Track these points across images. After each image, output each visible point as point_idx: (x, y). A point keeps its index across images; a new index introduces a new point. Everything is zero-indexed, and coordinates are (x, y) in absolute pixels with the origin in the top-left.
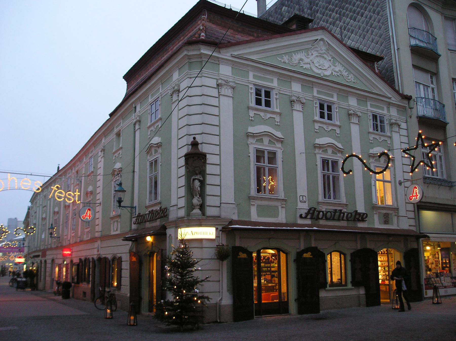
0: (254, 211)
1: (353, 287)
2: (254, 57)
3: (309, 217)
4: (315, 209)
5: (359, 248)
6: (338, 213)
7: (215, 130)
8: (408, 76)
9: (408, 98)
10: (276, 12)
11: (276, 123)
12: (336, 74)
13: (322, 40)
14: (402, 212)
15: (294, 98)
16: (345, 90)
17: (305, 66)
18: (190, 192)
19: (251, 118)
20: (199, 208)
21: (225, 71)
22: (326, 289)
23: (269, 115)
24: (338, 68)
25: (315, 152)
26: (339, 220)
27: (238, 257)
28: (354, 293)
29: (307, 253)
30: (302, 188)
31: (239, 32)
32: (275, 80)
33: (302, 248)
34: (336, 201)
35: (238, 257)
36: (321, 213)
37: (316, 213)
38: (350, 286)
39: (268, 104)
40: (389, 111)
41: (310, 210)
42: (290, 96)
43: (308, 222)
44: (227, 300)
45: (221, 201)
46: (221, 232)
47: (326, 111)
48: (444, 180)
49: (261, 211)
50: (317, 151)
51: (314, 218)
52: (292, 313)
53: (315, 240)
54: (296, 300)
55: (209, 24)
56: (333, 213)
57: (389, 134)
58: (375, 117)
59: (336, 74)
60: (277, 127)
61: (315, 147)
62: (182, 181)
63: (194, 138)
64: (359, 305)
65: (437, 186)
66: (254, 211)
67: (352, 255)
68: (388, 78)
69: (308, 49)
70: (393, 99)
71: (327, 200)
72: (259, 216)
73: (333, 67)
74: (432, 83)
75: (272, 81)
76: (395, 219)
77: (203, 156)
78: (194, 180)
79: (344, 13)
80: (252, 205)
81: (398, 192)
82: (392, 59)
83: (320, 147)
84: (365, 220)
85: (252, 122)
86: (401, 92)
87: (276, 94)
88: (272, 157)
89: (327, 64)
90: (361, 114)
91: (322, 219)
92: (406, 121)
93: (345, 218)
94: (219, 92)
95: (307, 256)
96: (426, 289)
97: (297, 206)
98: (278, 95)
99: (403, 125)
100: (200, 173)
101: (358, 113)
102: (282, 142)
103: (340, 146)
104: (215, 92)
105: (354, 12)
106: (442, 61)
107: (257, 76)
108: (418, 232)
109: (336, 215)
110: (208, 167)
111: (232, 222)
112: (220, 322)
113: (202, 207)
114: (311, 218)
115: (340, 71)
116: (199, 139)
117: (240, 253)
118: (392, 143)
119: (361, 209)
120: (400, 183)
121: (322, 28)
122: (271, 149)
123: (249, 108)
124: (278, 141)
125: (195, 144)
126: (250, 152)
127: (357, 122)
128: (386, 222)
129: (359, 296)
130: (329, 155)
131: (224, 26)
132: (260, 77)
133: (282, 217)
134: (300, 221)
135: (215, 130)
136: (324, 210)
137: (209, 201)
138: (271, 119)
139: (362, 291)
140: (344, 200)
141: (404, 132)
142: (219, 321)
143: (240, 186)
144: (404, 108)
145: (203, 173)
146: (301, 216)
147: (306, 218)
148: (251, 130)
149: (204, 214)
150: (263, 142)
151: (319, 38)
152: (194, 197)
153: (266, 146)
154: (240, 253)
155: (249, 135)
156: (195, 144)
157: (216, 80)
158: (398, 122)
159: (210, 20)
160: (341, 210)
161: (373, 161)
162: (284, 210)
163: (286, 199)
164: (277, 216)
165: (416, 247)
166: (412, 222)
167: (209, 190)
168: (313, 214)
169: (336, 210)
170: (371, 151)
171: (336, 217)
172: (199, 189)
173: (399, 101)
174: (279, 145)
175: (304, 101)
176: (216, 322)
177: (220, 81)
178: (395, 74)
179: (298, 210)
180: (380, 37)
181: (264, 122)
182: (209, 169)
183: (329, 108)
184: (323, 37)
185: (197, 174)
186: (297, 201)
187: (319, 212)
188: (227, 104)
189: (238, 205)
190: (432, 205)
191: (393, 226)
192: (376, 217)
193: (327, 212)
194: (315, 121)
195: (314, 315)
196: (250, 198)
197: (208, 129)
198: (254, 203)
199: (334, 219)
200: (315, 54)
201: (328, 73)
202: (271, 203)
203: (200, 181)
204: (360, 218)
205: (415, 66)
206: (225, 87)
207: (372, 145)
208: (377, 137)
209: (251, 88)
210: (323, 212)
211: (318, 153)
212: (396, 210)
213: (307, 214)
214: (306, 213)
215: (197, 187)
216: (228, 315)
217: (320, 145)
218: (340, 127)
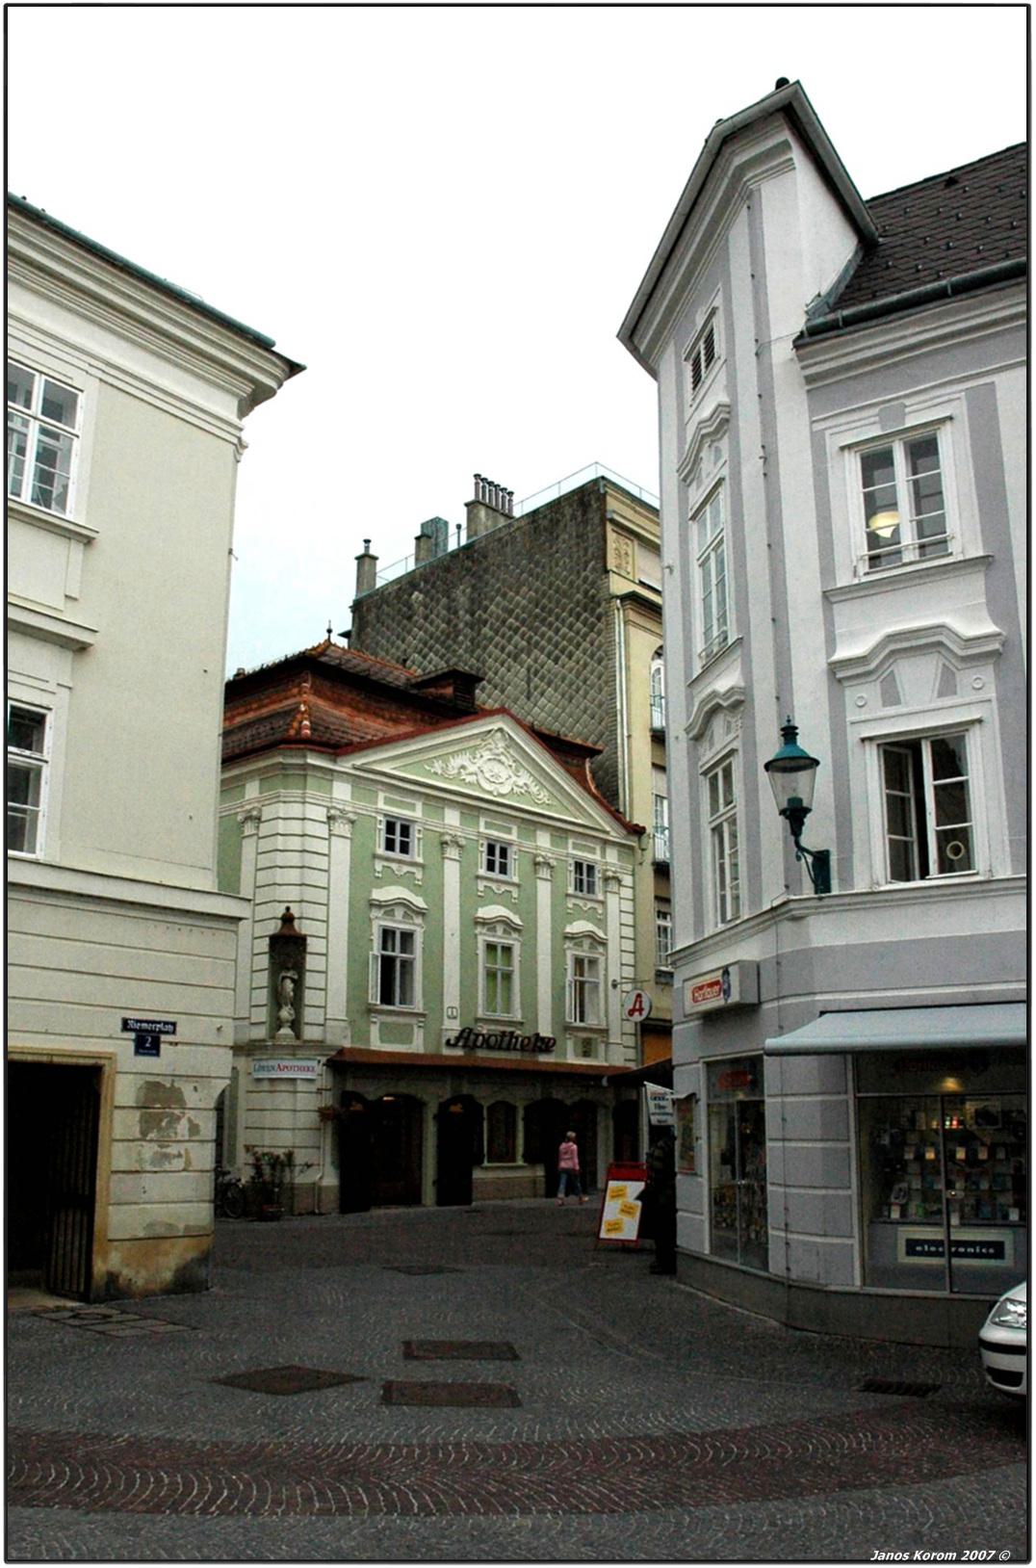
0: (374, 1031)
2: (386, 768)
5: (539, 1097)
7: (321, 895)
9: (638, 831)
10: (398, 597)
13: (500, 730)
14: (615, 1037)
15: (447, 838)
16: (531, 822)
17: (469, 779)
18: (277, 999)
21: (342, 791)
24: (524, 779)
26: (508, 1049)
28: (527, 1173)
30: (452, 997)
31: (359, 710)
32: (419, 805)
33: (448, 1096)
34: (505, 1017)
38: (520, 1162)
39: (405, 848)
40: (603, 855)
42: (442, 834)
43: (459, 1052)
44: (330, 1179)
47: (497, 856)
49: (386, 1033)
50: (479, 929)
55: (312, 699)
57: (600, 897)
58: (579, 866)
60: (416, 889)
61: (477, 923)
62: (263, 979)
66: (374, 1031)
67: (526, 1109)
68: (607, 793)
69: (476, 747)
71: (490, 1015)
75: (412, 807)
76: (602, 1047)
77: (300, 941)
79: (537, 643)
85: (380, 882)
88: (407, 937)
89: (504, 773)
99: (628, 880)
103: (518, 921)
104: (322, 830)
105: (556, 646)
109: (504, 1041)
110: (308, 958)
111: (341, 1051)
113: (296, 1025)
116: (295, 911)
118: (605, 913)
119: (545, 1031)
120: (615, 986)
121: (502, 711)
123: (375, 856)
124: (516, 930)
125: (288, 919)
128: (586, 1054)
129: (534, 1182)
131: (338, 702)
133: (417, 1044)
134: (446, 1051)
135: (321, 895)
137: (309, 1014)
139: (540, 1172)
140: (518, 1016)
143: (356, 988)
144: (631, 848)
145: (299, 967)
146: (448, 1043)
147: (455, 1045)
149: (298, 1036)
151: (495, 727)
153: (399, 924)
155: (373, 905)
156: (288, 919)
159: (317, 692)
164: (409, 1040)
167: (309, 997)
169: (504, 1033)
170: (569, 929)
174: (418, 920)
180: (600, 706)
181: (397, 880)
182: (311, 962)
183: (504, 853)
184: (500, 725)
188: (342, 850)
192: (570, 1045)
196: (370, 1010)
197: (310, 894)
199: (500, 1048)
200: (487, 755)
201: (505, 790)
202: (402, 1020)
203: (293, 981)
207: (570, 918)
208: (581, 903)
212: (605, 1032)
213: (458, 1039)
216: (331, 1201)
218: (518, 886)
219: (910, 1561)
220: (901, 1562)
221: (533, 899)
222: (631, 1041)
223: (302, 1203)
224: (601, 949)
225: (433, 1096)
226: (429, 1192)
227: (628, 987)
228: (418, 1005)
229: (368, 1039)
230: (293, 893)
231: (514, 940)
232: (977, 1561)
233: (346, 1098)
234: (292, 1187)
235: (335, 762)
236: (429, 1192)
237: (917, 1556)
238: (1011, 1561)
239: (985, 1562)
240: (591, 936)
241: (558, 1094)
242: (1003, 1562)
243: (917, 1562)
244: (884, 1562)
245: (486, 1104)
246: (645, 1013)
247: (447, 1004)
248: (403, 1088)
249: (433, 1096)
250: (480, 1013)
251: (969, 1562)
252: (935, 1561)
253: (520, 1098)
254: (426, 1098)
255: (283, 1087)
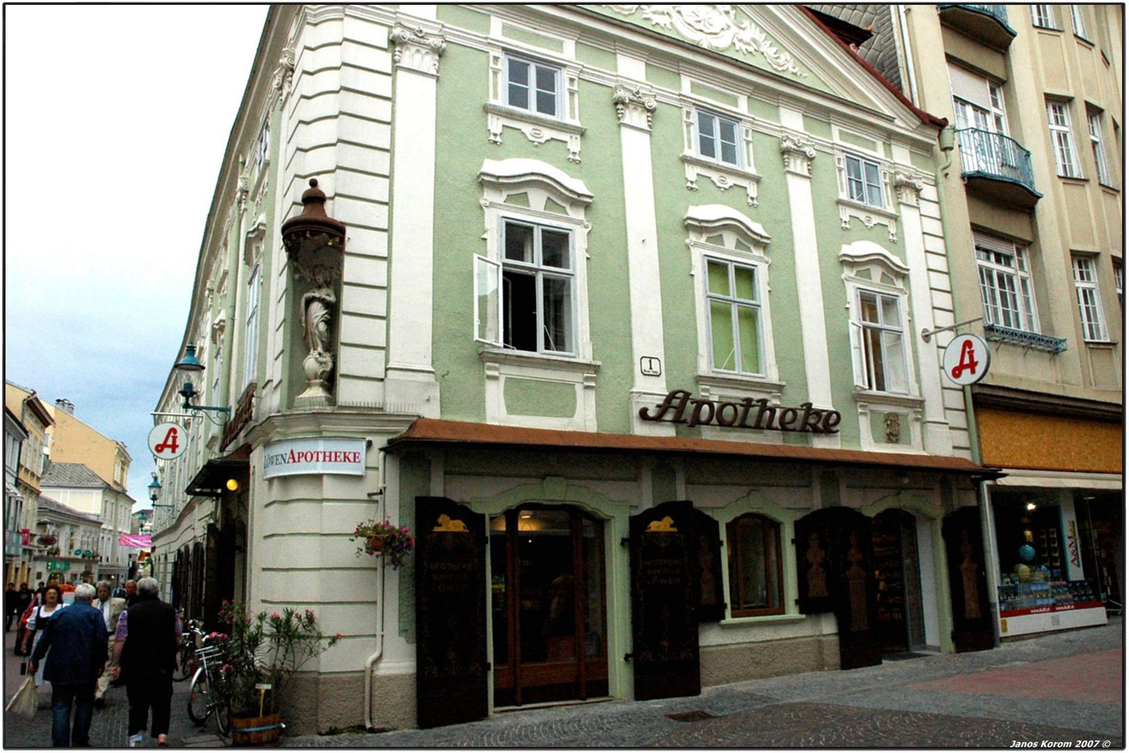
1: (804, 616)
3: (669, 416)
4: (687, 395)
6: (757, 409)
8: (936, 80)
9: (939, 125)
11: (571, 156)
12: (744, 47)
14: (934, 411)
16: (771, 88)
18: (300, 338)
19: (492, 138)
20: (322, 385)
22: (723, 622)
23: (547, 134)
25: (687, 241)
26: (758, 427)
27: (437, 529)
28: (806, 630)
29: (660, 519)
30: (648, 336)
33: (647, 503)
34: (748, 376)
35: (437, 529)
36: (706, 408)
37: (690, 407)
38: (792, 612)
41: (672, 396)
43: (665, 431)
44: (398, 661)
45: (387, 362)
46: (382, 454)
48: (1033, 337)
49: (517, 397)
50: (693, 237)
51: (685, 421)
52: (618, 695)
53: (689, 482)
54: (627, 657)
56: (740, 409)
57: (891, 210)
59: (744, 47)
60: (574, 164)
61: (688, 228)
63: (314, 184)
64: (821, 666)
65: (1020, 350)
67: (797, 525)
68: (887, 75)
70: (897, 121)
72: (511, 410)
73: (734, 29)
74: (995, 104)
76: (915, 429)
78: (309, 302)
80: (489, 377)
81: (922, 360)
82: (892, 36)
83: (700, 227)
84: (834, 429)
86: (917, 105)
87: (572, 80)
90: (814, 153)
91: (707, 423)
92: (936, 181)
93: (776, 423)
94: (394, 62)
95: (662, 529)
96: (1004, 614)
97: (632, 387)
98: (576, 83)
99: (929, 192)
100: (328, 284)
101: (806, 149)
102: (587, 207)
103: (757, 228)
104: (383, 61)
106: (1018, 48)
107: (512, 29)
108: (978, 463)
109: (751, 414)
111: (417, 422)
112: (372, 730)
113: (330, 381)
114: (677, 421)
115: (755, 41)
116: (326, 186)
117: (443, 518)
118: (900, 233)
119: (822, 400)
120: (927, 338)
122: (555, 223)
124: (757, 244)
125: (314, 199)
126: (487, 226)
127: (806, 173)
128: (892, 438)
129: (819, 643)
130: (729, 253)
132: (523, 32)
133: (583, 418)
134: (641, 430)
136: (716, 398)
137: (349, 361)
138: (553, 143)
139: (828, 627)
141: (933, 210)
142: (368, 725)
144: (928, 148)
146: (643, 414)
147: (658, 419)
148: (492, 167)
149: (332, 401)
150: (527, 202)
152: (308, 352)
154: (443, 518)
155: (486, 183)
156: (314, 199)
157: (386, 30)
158: (914, 181)
160: (764, 402)
161: (853, 275)
162: (592, 394)
163: (599, 363)
164: (568, 410)
165: (974, 503)
166: (962, 439)
167: (349, 328)
168: (680, 409)
169: (748, 403)
170: (847, 249)
171: (751, 421)
172: (322, 327)
173: (914, 131)
175: (652, 103)
176: (361, 728)
177: (397, 31)
178: (902, 73)
179: (635, 398)
181: (535, 148)
182: (352, 269)
185: (320, 287)
186: (632, 371)
187: (700, 404)
188: (418, 99)
189: (443, 378)
190: (1012, 395)
191: (911, 448)
192: (864, 424)
193: (724, 406)
194: (685, 160)
195: (679, 704)
196: (483, 356)
197: (353, 157)
198: (496, 373)
199: (743, 426)
204: (820, 425)
205: (951, 59)
206: (413, 49)
209: (496, 59)
210: (711, 404)
211: (696, 245)
212: (919, 404)
214: (658, 406)
215: (315, 321)
216: (399, 704)
217: (700, 221)
219: (1039, 748)
220: (1032, 748)
221: (784, 203)
222: (959, 420)
223: (335, 710)
224: (899, 284)
225: (618, 505)
226: (620, 676)
227: (945, 338)
228: (582, 346)
229: (480, 405)
230: (325, 159)
231: (753, 258)
232: (1086, 748)
233: (426, 510)
234: (317, 680)
235: (793, 541)
236: (620, 676)
237: (1044, 744)
238: (1112, 748)
239: (1092, 748)
240: (881, 261)
241: (849, 499)
242: (1105, 749)
243: (1044, 748)
244: (1020, 749)
245: (723, 520)
246: (980, 369)
247: (636, 352)
248: (555, 492)
249: (618, 505)
250: (704, 368)
251: (1081, 748)
252: (1056, 748)
253: (786, 507)
254: (604, 510)
255: (300, 491)
